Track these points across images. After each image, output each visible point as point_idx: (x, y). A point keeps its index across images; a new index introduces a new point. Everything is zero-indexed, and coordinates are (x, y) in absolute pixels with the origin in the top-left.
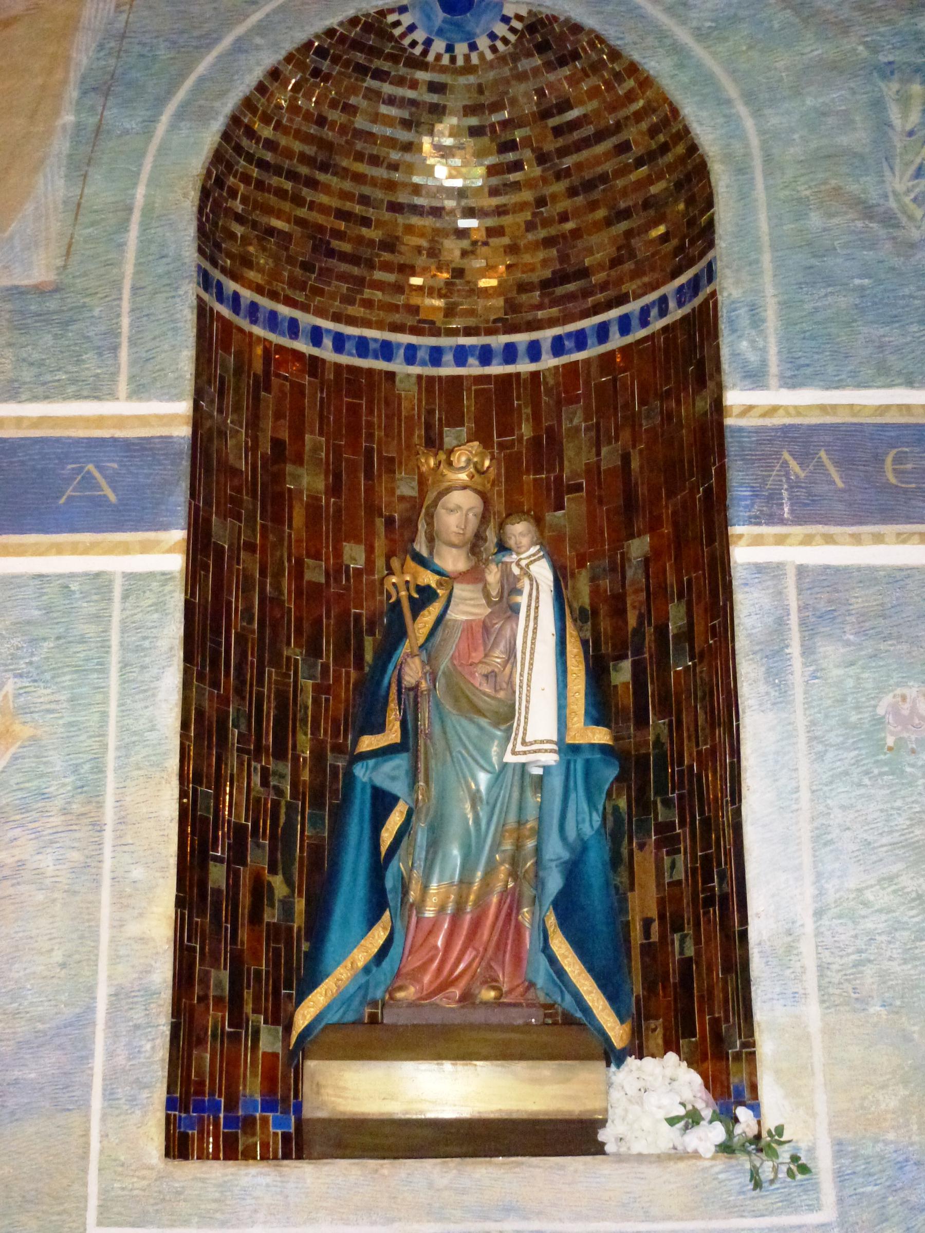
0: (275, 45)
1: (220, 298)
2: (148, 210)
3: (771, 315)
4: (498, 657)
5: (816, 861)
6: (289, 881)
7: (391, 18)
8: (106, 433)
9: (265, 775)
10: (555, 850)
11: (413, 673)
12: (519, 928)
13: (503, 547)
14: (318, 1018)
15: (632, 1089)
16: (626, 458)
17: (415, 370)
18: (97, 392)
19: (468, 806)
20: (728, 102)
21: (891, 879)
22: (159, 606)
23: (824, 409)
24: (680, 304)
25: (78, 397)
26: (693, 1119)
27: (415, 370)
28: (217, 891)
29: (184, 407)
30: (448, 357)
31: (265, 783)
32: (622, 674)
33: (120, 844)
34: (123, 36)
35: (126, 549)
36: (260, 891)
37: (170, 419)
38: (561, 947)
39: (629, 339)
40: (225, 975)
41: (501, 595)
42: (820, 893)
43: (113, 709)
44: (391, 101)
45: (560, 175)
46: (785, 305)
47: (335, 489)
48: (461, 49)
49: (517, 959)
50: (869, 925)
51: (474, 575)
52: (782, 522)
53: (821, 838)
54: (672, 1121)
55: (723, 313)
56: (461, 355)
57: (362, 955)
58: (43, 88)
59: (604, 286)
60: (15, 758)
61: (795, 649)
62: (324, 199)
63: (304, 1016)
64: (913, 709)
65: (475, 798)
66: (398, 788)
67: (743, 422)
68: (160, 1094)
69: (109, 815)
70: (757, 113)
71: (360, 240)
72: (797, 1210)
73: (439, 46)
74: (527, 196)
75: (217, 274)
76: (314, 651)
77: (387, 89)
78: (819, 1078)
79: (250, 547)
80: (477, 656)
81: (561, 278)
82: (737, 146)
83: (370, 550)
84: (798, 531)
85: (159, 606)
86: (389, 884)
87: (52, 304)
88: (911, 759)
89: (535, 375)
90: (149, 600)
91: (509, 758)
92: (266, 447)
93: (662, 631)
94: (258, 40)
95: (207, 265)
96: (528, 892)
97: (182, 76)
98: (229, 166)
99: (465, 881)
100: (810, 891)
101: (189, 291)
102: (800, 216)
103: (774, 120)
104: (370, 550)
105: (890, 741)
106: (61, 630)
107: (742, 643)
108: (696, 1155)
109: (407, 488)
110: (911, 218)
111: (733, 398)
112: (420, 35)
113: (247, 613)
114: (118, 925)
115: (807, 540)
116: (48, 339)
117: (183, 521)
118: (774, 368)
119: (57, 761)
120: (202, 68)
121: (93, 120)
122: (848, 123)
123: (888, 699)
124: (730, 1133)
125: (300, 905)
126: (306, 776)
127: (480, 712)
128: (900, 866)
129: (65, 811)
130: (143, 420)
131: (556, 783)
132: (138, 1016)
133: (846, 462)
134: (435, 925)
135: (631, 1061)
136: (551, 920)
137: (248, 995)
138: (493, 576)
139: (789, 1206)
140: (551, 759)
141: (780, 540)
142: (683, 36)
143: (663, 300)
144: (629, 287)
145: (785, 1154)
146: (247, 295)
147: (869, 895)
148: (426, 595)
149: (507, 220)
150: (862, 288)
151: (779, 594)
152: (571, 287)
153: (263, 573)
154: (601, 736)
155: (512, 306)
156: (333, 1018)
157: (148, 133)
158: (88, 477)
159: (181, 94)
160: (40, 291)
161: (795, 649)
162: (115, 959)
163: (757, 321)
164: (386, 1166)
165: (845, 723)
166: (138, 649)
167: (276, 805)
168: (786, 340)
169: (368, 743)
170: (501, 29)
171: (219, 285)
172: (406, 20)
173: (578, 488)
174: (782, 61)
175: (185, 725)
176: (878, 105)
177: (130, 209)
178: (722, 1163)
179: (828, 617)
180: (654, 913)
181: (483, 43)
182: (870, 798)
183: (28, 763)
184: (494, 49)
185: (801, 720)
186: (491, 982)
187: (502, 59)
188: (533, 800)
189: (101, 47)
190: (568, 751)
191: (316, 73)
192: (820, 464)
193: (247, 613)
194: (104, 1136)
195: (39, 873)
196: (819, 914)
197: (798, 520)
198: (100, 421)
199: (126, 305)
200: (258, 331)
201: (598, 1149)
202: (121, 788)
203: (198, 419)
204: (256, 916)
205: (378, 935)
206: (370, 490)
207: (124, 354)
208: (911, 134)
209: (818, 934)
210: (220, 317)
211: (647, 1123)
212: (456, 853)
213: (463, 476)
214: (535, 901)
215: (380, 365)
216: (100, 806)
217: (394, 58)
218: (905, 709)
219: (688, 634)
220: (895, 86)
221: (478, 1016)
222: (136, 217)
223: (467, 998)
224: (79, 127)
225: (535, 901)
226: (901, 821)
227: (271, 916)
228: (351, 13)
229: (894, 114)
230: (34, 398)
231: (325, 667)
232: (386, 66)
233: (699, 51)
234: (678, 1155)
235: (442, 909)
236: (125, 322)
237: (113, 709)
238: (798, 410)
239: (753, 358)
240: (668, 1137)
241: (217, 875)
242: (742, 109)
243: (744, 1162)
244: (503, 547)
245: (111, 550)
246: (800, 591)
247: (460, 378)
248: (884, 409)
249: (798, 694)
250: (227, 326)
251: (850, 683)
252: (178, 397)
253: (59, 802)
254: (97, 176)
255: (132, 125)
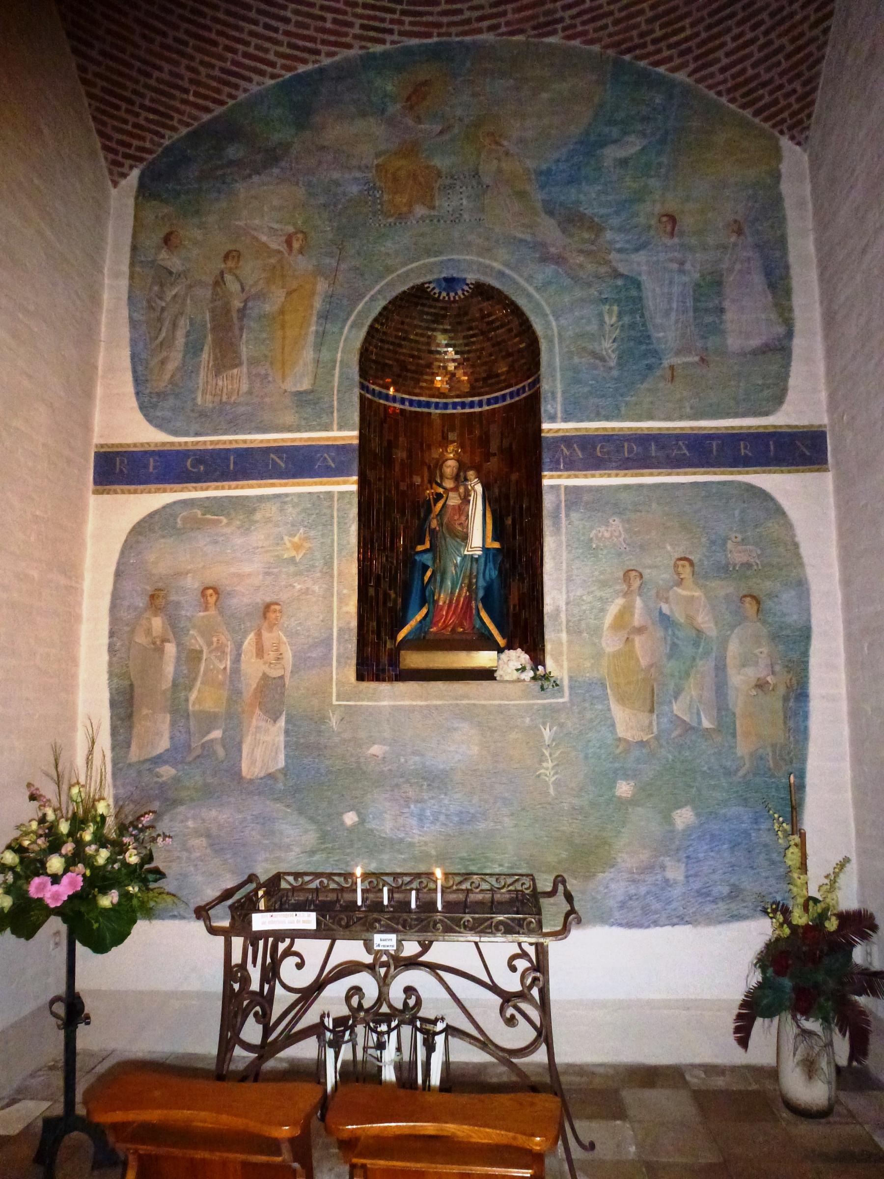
0: (385, 298)
1: (368, 392)
2: (341, 361)
3: (559, 395)
4: (463, 518)
5: (567, 587)
6: (396, 593)
7: (426, 286)
8: (330, 443)
9: (387, 557)
10: (482, 583)
11: (434, 524)
12: (471, 607)
13: (466, 479)
14: (405, 637)
15: (506, 660)
16: (511, 445)
17: (438, 411)
18: (327, 427)
19: (453, 568)
20: (547, 315)
21: (592, 592)
22: (350, 503)
23: (576, 429)
24: (530, 390)
25: (320, 430)
26: (523, 669)
27: (438, 411)
28: (372, 597)
29: (356, 433)
30: (450, 406)
31: (387, 560)
32: (509, 521)
33: (339, 582)
34: (331, 297)
35: (338, 483)
36: (386, 596)
37: (352, 438)
38: (484, 615)
39: (513, 401)
40: (375, 624)
41: (465, 496)
42: (568, 597)
43: (336, 537)
44: (427, 314)
45: (489, 339)
46: (563, 392)
47: (410, 456)
48: (452, 294)
49: (470, 617)
50: (584, 608)
51: (455, 489)
52: (560, 470)
53: (569, 579)
54: (517, 670)
55: (542, 396)
56: (455, 406)
57: (419, 617)
58: (304, 317)
59: (505, 380)
60: (305, 554)
61: (563, 515)
62: (404, 351)
63: (401, 635)
64: (603, 535)
65: (456, 565)
66: (429, 563)
67: (548, 435)
68: (354, 661)
69: (336, 573)
70: (557, 319)
71: (418, 365)
72: (556, 698)
73: (444, 294)
74: (478, 346)
75: (366, 383)
76: (403, 514)
77: (426, 309)
78: (565, 657)
79: (380, 479)
80: (456, 517)
81: (489, 377)
82: (549, 333)
83: (422, 478)
84: (566, 473)
85: (350, 503)
86: (427, 594)
87: (311, 397)
88: (601, 552)
89: (481, 412)
90: (346, 500)
91: (466, 553)
92: (385, 444)
93: (521, 507)
94: (379, 297)
95: (362, 381)
96: (474, 596)
97: (352, 311)
98: (373, 337)
99: (452, 593)
100: (565, 597)
101: (357, 391)
102: (571, 358)
103: (563, 322)
104: (422, 478)
105: (594, 546)
106: (317, 511)
107: (545, 513)
108: (524, 680)
109: (435, 455)
110: (610, 358)
111: (545, 426)
112: (437, 291)
113: (379, 501)
114: (339, 608)
115: (569, 477)
116: (310, 410)
117: (357, 473)
118: (559, 415)
119: (318, 555)
120: (360, 307)
121: (321, 329)
122: (589, 322)
123: (594, 532)
124: (535, 674)
125: (400, 600)
126: (401, 557)
127: (457, 537)
128: (595, 588)
129: (321, 572)
130: (342, 438)
131: (482, 560)
132: (346, 637)
133: (583, 448)
134: (442, 607)
135: (506, 651)
136: (480, 606)
137: (382, 629)
138: (462, 490)
139: (553, 696)
140: (480, 553)
141: (559, 477)
142: (531, 290)
143: (524, 387)
144: (513, 381)
145: (552, 680)
146: (377, 388)
147: (584, 598)
148: (439, 496)
149: (471, 355)
150: (592, 385)
151: (558, 496)
152: (493, 381)
153: (385, 489)
154: (497, 545)
155: (472, 387)
156: (410, 637)
157: (341, 333)
158: (325, 459)
159: (352, 318)
160: (305, 392)
161: (563, 515)
162: (338, 619)
163: (554, 398)
164: (425, 684)
165: (578, 540)
166: (343, 517)
167: (391, 568)
168: (564, 405)
169: (420, 548)
170: (466, 288)
171: (368, 387)
172: (432, 286)
173: (495, 454)
174: (567, 299)
175: (359, 543)
176: (600, 315)
177: (335, 362)
178: (532, 684)
179: (575, 503)
180: (517, 602)
181: (460, 292)
182: (586, 565)
183: (308, 556)
184: (463, 294)
185: (564, 538)
186: (462, 626)
187: (466, 297)
188: (475, 566)
189: (324, 301)
190: (485, 549)
191: (400, 306)
192: (574, 450)
193: (379, 501)
194: (337, 674)
195: (314, 592)
196: (567, 604)
197: (566, 469)
198: (328, 439)
199: (335, 397)
200: (382, 401)
201: (494, 679)
202: (339, 564)
203: (362, 437)
204: (385, 603)
205: (424, 611)
206: (422, 456)
207: (335, 414)
208: (612, 326)
209: (567, 610)
210: (368, 399)
211: (509, 671)
212: (449, 583)
213: (452, 455)
214: (476, 600)
215: (426, 410)
216: (333, 569)
217: (427, 299)
218: (600, 535)
219: (529, 508)
220: (607, 307)
221: (456, 637)
222: (338, 364)
223: (453, 630)
224: (317, 332)
225: (476, 600)
226: (596, 573)
227: (390, 604)
228: (411, 284)
229: (607, 319)
230: (306, 431)
231: (407, 520)
232: (425, 301)
233: (537, 296)
234: (519, 680)
235: (445, 603)
236: (335, 403)
237: (336, 537)
238: (567, 430)
239: (552, 411)
240: (515, 675)
241: (372, 592)
242: (551, 318)
243: (540, 683)
244: (466, 479)
245: (333, 484)
246: (566, 494)
247: (454, 414)
248: (597, 429)
249: (564, 530)
250: (371, 401)
251: (581, 527)
252: (353, 430)
253: (318, 569)
254: (324, 350)
255: (336, 330)
